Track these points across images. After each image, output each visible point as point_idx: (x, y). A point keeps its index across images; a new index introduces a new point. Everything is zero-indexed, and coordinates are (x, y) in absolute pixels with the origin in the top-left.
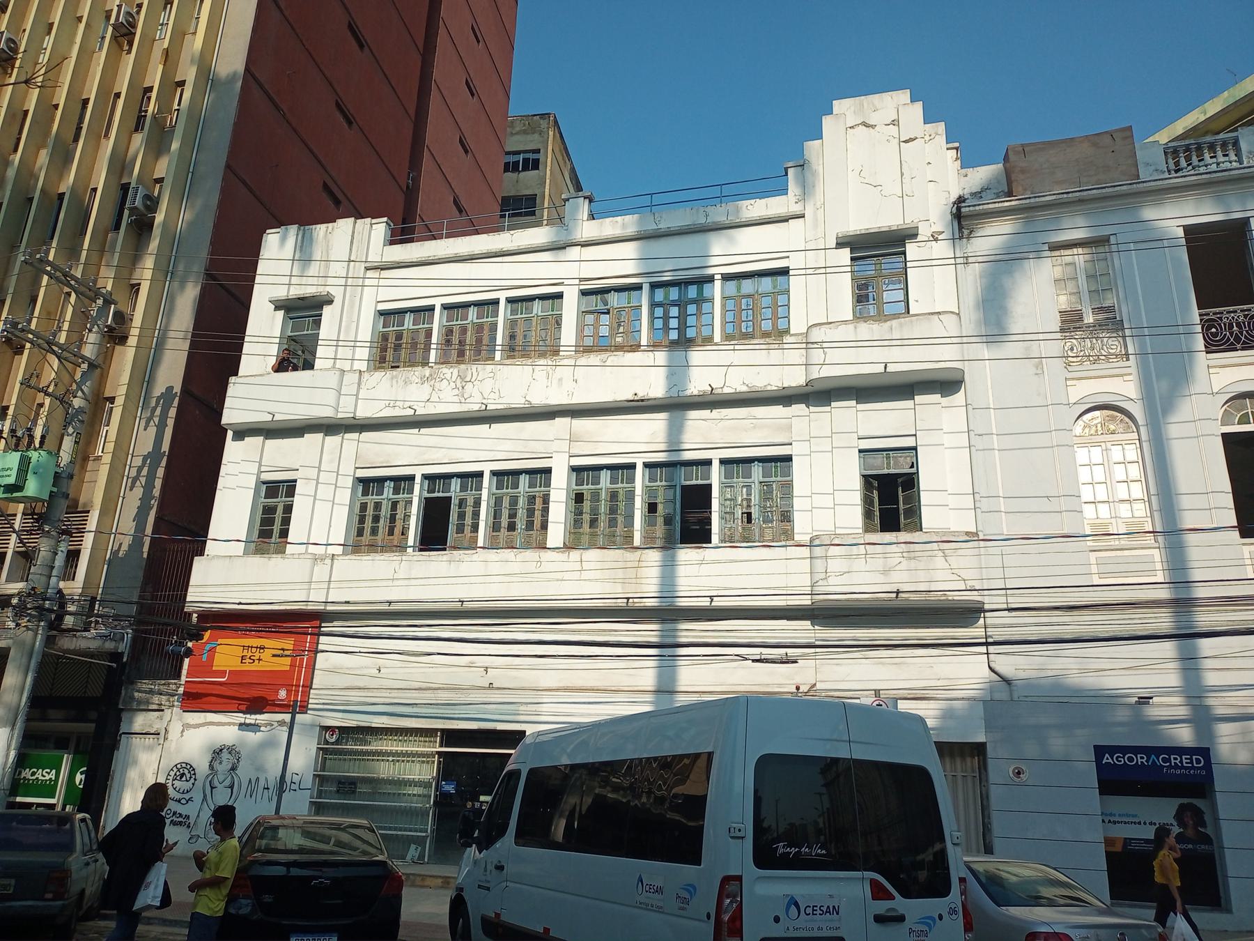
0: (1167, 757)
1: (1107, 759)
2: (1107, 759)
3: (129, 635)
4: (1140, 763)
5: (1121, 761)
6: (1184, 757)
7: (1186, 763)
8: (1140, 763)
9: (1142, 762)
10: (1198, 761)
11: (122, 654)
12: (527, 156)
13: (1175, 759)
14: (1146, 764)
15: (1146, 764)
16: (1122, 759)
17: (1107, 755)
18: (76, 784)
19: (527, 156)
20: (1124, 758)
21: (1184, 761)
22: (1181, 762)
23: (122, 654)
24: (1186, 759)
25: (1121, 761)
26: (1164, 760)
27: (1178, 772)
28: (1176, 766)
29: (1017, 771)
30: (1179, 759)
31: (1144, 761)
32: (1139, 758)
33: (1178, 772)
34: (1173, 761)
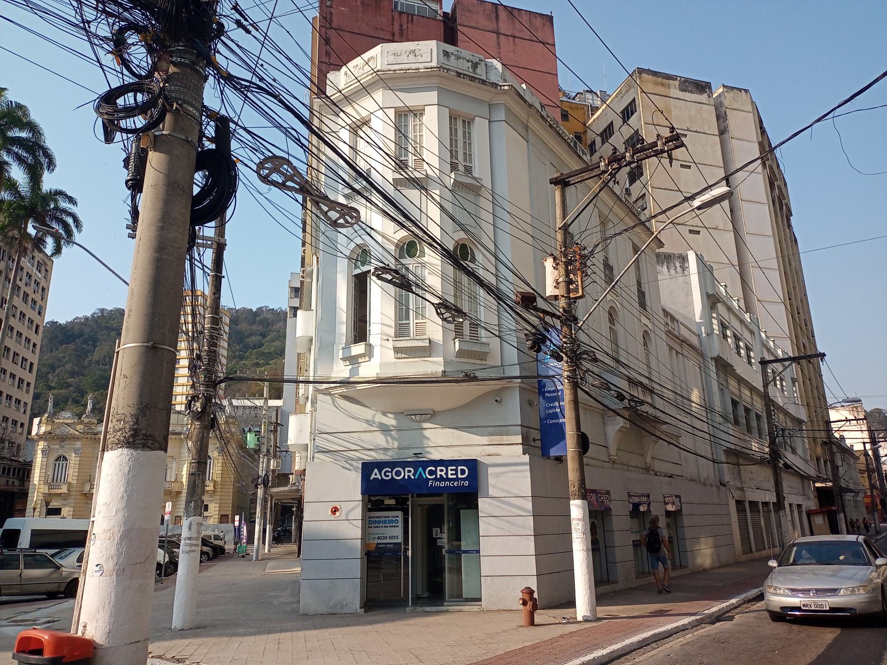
0: (434, 469)
1: (375, 474)
2: (376, 474)
4: (406, 478)
5: (388, 476)
6: (450, 468)
7: (451, 474)
8: (406, 478)
9: (409, 476)
10: (463, 472)
15: (413, 478)
16: (390, 474)
17: (376, 471)
20: (391, 472)
21: (450, 472)
22: (446, 474)
24: (451, 470)
25: (388, 476)
26: (431, 472)
27: (442, 484)
28: (441, 479)
30: (413, 470)
31: (411, 474)
33: (442, 484)
34: (439, 473)
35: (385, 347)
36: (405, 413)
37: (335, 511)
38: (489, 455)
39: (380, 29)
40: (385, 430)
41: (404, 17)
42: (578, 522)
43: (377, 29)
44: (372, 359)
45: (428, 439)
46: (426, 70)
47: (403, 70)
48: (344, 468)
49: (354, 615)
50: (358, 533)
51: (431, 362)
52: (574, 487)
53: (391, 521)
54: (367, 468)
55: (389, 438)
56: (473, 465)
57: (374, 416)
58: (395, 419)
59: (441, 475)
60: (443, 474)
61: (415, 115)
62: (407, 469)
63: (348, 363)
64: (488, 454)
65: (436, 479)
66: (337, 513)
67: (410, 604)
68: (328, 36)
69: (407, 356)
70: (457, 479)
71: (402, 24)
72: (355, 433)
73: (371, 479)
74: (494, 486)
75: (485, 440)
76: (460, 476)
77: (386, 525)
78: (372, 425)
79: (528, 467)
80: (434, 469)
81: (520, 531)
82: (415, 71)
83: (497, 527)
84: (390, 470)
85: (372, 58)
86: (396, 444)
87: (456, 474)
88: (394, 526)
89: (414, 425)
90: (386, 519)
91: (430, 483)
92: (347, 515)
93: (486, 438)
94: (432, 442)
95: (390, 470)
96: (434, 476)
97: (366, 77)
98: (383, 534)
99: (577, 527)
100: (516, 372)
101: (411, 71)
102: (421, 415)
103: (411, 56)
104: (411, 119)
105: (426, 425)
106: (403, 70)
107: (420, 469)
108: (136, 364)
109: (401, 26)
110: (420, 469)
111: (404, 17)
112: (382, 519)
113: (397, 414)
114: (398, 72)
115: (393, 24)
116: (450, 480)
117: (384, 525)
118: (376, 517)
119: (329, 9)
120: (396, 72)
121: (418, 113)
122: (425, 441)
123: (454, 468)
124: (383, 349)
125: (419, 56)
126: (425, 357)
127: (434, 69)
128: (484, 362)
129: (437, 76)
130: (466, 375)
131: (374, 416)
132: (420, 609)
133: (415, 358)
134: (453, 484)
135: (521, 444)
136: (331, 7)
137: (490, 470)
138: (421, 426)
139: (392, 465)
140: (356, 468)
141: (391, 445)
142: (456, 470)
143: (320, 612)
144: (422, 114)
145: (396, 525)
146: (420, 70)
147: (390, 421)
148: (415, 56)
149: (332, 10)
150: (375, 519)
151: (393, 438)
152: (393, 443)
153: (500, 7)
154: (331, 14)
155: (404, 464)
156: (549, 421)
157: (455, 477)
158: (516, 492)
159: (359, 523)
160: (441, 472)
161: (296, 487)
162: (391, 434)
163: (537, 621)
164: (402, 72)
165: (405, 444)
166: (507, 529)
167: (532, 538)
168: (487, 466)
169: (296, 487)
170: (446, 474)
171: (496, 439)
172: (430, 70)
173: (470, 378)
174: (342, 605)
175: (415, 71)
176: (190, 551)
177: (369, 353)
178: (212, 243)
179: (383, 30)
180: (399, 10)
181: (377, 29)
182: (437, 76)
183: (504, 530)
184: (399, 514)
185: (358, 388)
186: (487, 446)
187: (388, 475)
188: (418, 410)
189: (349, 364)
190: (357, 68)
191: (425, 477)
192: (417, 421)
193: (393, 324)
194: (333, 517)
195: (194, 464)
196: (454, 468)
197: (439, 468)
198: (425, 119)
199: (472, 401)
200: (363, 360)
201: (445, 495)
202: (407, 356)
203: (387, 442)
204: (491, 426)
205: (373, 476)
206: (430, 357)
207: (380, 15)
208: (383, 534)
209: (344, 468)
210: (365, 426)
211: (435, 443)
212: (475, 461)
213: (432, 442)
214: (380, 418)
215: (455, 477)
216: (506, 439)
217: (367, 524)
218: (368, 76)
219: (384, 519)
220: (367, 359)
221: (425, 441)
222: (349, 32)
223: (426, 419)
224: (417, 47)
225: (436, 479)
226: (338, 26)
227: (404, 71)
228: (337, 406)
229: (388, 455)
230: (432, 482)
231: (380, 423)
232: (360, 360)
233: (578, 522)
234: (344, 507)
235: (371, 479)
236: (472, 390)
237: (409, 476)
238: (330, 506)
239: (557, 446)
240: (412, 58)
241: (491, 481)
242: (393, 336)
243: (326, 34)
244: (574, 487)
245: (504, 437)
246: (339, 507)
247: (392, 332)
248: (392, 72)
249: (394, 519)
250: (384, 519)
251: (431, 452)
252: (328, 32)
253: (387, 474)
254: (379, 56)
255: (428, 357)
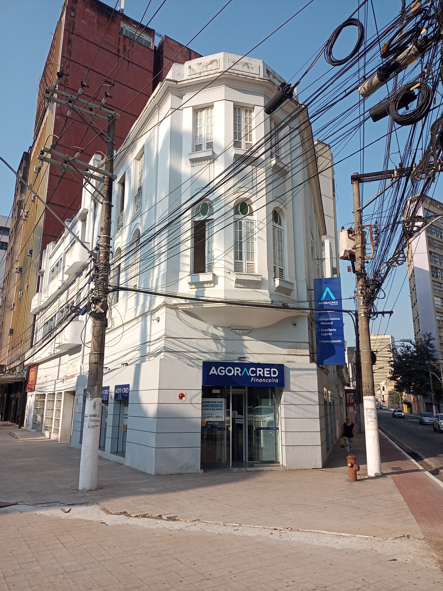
0: (255, 369)
1: (213, 371)
2: (213, 371)
3: (385, 59)
4: (236, 375)
5: (222, 373)
6: (266, 369)
7: (267, 374)
8: (236, 375)
9: (237, 373)
10: (274, 373)
11: (25, 378)
12: (295, 286)
13: (238, 370)
14: (240, 375)
15: (240, 375)
16: (224, 371)
17: (213, 368)
18: (168, 266)
19: (295, 286)
20: (225, 370)
21: (266, 372)
22: (263, 373)
23: (25, 378)
24: (267, 371)
25: (222, 373)
26: (253, 372)
27: (261, 381)
29: (181, 396)
30: (240, 370)
31: (239, 372)
32: (235, 370)
34: (258, 372)
35: (227, 278)
36: (231, 328)
37: (182, 396)
38: (288, 362)
39: (109, 44)
40: (216, 339)
41: (127, 40)
42: (371, 411)
43: (107, 43)
44: (216, 286)
45: (246, 347)
46: (260, 80)
47: (244, 75)
48: (189, 365)
49: (195, 475)
50: (199, 413)
51: (260, 292)
52: (368, 387)
53: (217, 406)
54: (207, 366)
55: (219, 345)
56: (281, 367)
57: (208, 328)
58: (223, 331)
59: (260, 374)
60: (261, 373)
61: (246, 111)
62: (236, 368)
63: (194, 286)
64: (287, 361)
65: (256, 377)
66: (183, 398)
67: (231, 466)
68: (70, 39)
69: (244, 286)
70: (271, 377)
71: (126, 45)
72: (194, 340)
73: (210, 374)
74: (293, 384)
75: (285, 351)
76: (272, 375)
77: (214, 408)
78: (206, 335)
79: (316, 372)
80: (255, 369)
81: (310, 415)
82: (252, 78)
83: (296, 412)
84: (224, 368)
85: (215, 60)
86: (224, 350)
87: (270, 374)
88: (220, 409)
89: (237, 337)
90: (214, 403)
91: (252, 380)
92: (192, 399)
93: (286, 350)
94: (249, 350)
95: (224, 368)
96: (255, 375)
97: (214, 74)
98: (211, 415)
99: (371, 414)
100: (307, 305)
101: (249, 78)
102: (244, 330)
103: (245, 66)
104: (243, 113)
105: (245, 338)
106: (244, 75)
107: (245, 369)
108: (165, 268)
109: (125, 46)
110: (245, 369)
111: (127, 40)
112: (210, 404)
113: (225, 328)
114: (240, 76)
115: (119, 43)
116: (266, 378)
117: (212, 408)
118: (207, 402)
119: (73, 18)
120: (239, 75)
121: (249, 109)
122: (245, 349)
123: (269, 369)
124: (226, 279)
125: (251, 68)
126: (256, 288)
127: (265, 81)
128: (288, 297)
129: (266, 86)
130: (283, 304)
131: (208, 328)
132: (244, 469)
133: (249, 288)
134: (268, 381)
135: (309, 356)
136: (74, 17)
137: (292, 373)
138: (242, 338)
139: (225, 364)
140: (197, 366)
141: (220, 350)
142: (270, 371)
143: (170, 472)
144: (251, 112)
145: (221, 408)
146: (256, 79)
147: (220, 333)
148: (248, 67)
149: (75, 20)
150: (205, 403)
151: (222, 346)
152: (222, 349)
153: (192, 52)
154: (74, 22)
155: (234, 365)
156: (323, 341)
157: (269, 376)
158: (308, 388)
159: (200, 406)
160: (260, 372)
161: (21, 376)
162: (220, 342)
163: (358, 478)
164: (243, 76)
165: (230, 350)
166: (302, 413)
167: (318, 420)
168: (290, 369)
169: (21, 376)
170: (263, 373)
171: (293, 351)
172: (263, 80)
173: (285, 307)
174: (187, 467)
175: (252, 78)
176: (95, 426)
177: (215, 281)
178: (104, 177)
179: (111, 45)
180: (124, 34)
181: (107, 43)
182: (266, 86)
183: (300, 414)
184: (223, 400)
185: (204, 306)
186: (287, 356)
187: (222, 372)
188: (241, 326)
189: (195, 287)
190: (201, 65)
191: (248, 375)
192: (239, 334)
193: (233, 262)
194: (180, 401)
195: (96, 355)
196: (269, 369)
197: (258, 369)
198: (254, 114)
199: (278, 323)
200: (209, 285)
201: (247, 388)
202: (244, 286)
203: (218, 348)
204: (290, 342)
205: (211, 372)
206: (259, 289)
207: (110, 34)
208: (211, 415)
209: (189, 365)
210: (201, 335)
211: (251, 351)
212: (283, 365)
213: (249, 350)
214: (212, 330)
215: (269, 376)
216: (299, 352)
217: (204, 406)
218: (216, 73)
219: (212, 404)
220: (212, 285)
221: (245, 349)
222: (86, 40)
223: (246, 333)
224: (249, 62)
225: (256, 377)
226: (79, 33)
227: (245, 77)
228: (181, 318)
229: (217, 357)
230: (254, 379)
231: (213, 334)
232: (205, 285)
233: (371, 411)
234: (189, 394)
235: (210, 374)
236: (284, 314)
237: (237, 373)
238: (178, 393)
239: (330, 358)
240: (245, 69)
241: (292, 380)
242: (233, 270)
243: (69, 36)
244: (368, 387)
245: (298, 350)
246: (185, 394)
247: (232, 267)
248: (236, 75)
249: (219, 404)
250: (212, 404)
251: (249, 357)
252: (70, 35)
253: (222, 371)
254: (221, 61)
255: (258, 289)
